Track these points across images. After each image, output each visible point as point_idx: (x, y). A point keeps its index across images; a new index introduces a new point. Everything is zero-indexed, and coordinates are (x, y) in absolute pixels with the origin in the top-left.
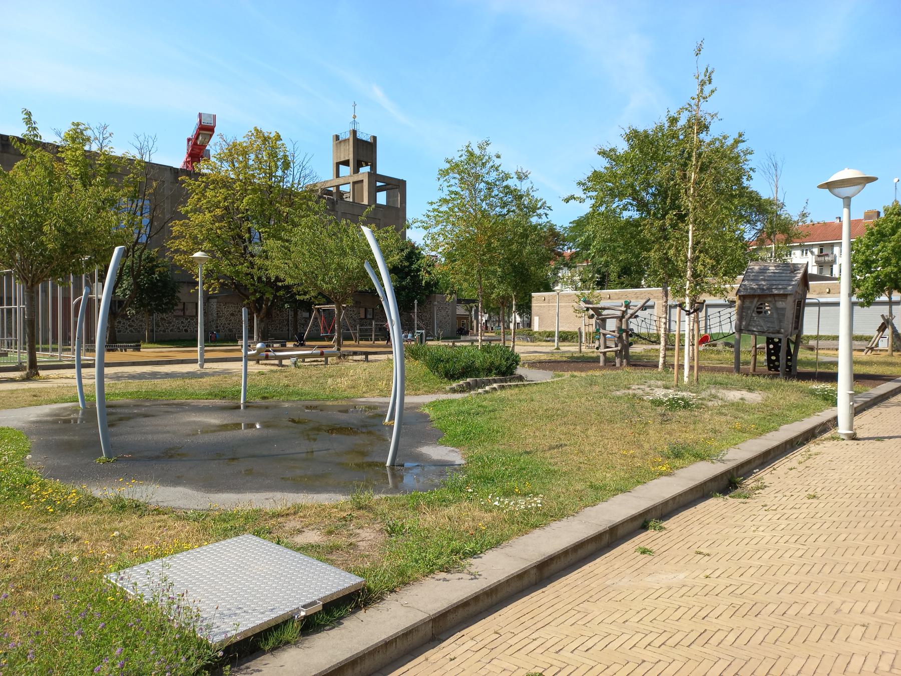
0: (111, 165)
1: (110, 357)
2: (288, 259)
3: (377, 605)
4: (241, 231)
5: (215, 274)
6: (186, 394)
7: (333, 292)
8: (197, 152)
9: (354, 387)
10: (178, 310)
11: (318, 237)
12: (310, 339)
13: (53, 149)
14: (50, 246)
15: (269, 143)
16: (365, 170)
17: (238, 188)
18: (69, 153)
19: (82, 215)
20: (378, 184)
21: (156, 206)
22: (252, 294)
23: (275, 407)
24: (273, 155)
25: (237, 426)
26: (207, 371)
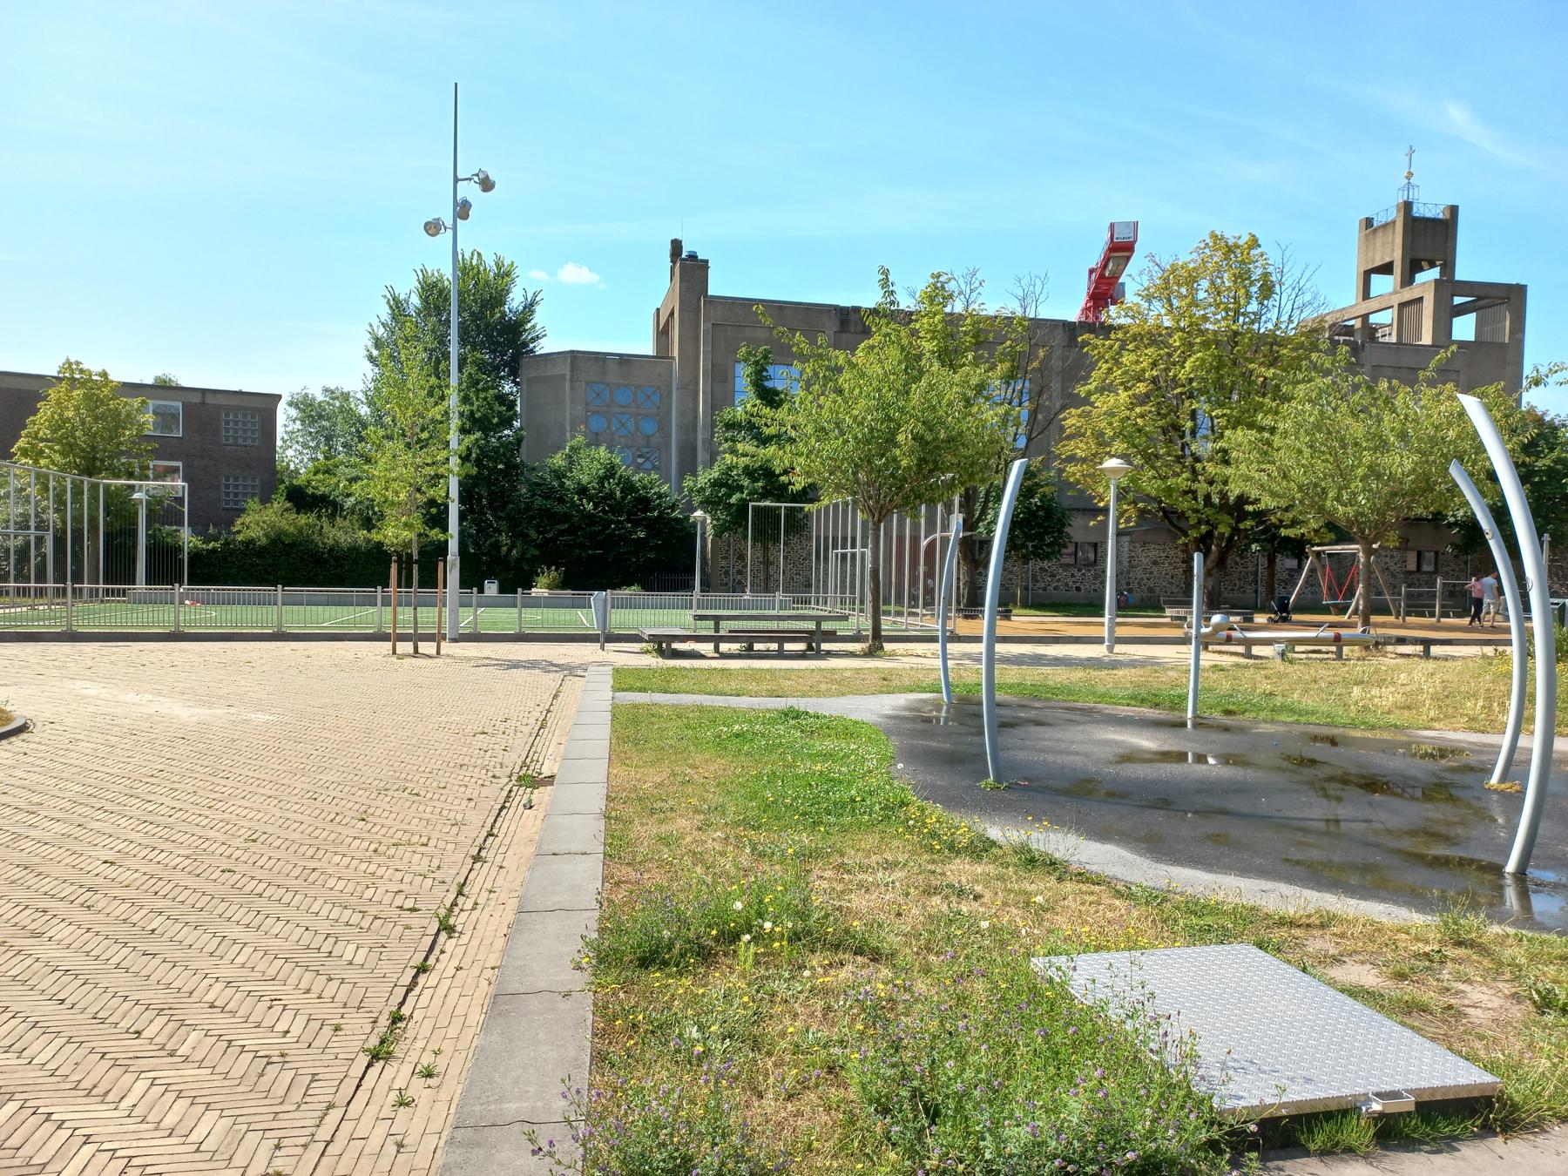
0: (980, 330)
1: (1003, 627)
2: (1269, 462)
3: (1531, 1137)
4: (1178, 417)
5: (1131, 494)
6: (1094, 694)
7: (1357, 521)
8: (1104, 290)
9: (1409, 708)
10: (1067, 554)
11: (1329, 419)
12: (1301, 608)
13: (907, 317)
14: (904, 463)
15: (1236, 257)
16: (1429, 276)
17: (1177, 344)
18: (925, 320)
19: (946, 413)
20: (1458, 300)
21: (1042, 388)
22: (1193, 527)
23: (1242, 730)
24: (1242, 277)
25: (1181, 757)
26: (1120, 658)
